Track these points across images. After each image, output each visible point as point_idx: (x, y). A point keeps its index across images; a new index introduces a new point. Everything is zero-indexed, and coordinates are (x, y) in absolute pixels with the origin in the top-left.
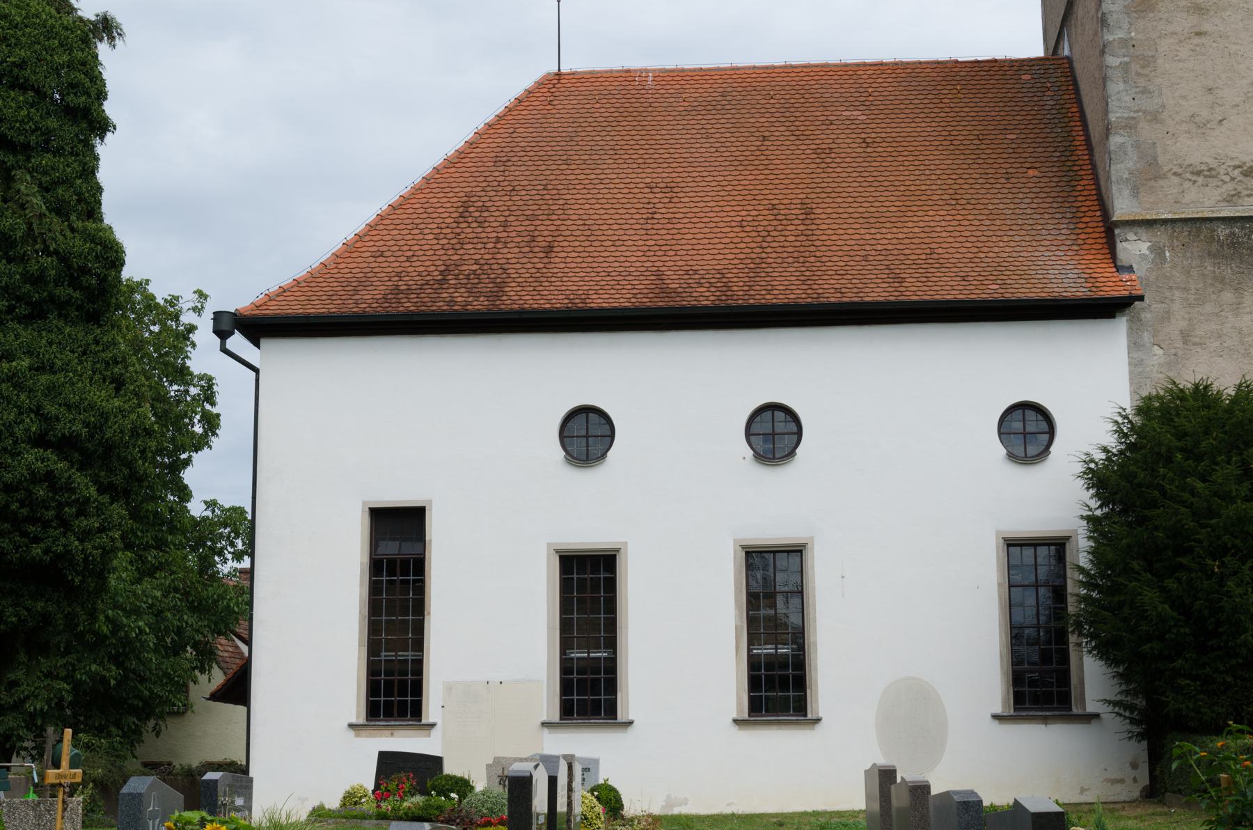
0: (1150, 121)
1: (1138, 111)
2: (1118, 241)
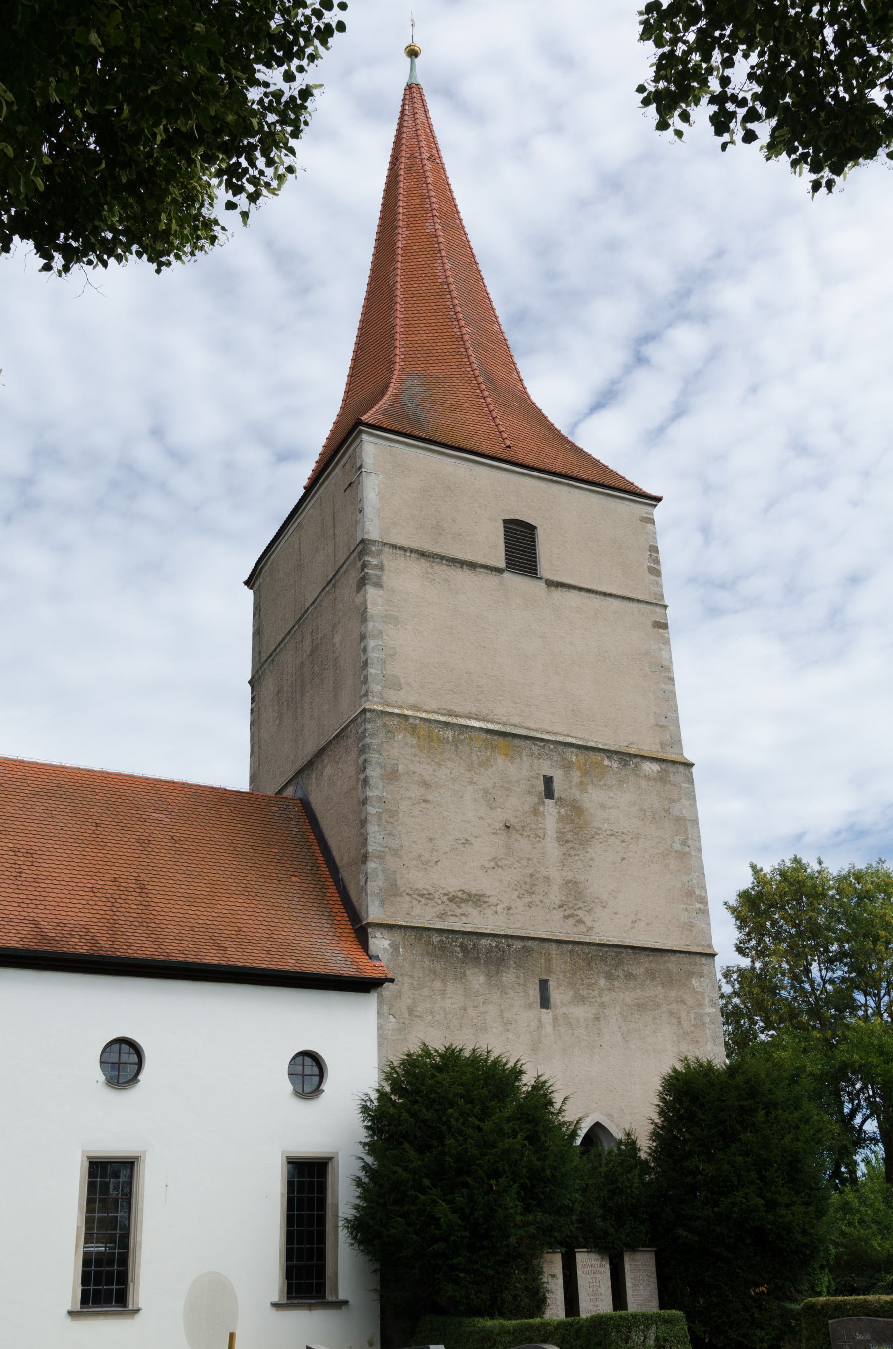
0: (394, 855)
1: (384, 847)
2: (370, 937)
